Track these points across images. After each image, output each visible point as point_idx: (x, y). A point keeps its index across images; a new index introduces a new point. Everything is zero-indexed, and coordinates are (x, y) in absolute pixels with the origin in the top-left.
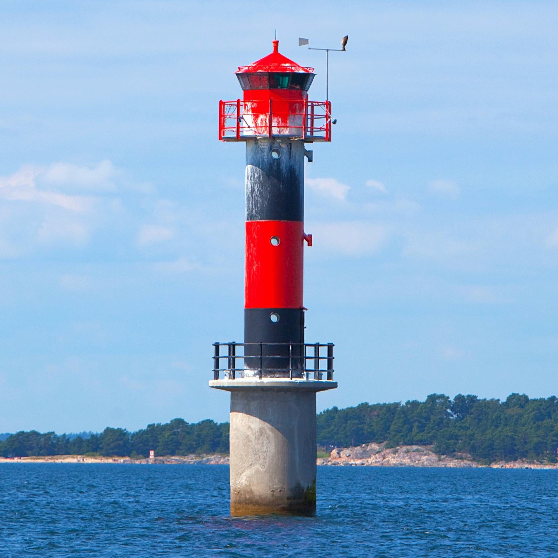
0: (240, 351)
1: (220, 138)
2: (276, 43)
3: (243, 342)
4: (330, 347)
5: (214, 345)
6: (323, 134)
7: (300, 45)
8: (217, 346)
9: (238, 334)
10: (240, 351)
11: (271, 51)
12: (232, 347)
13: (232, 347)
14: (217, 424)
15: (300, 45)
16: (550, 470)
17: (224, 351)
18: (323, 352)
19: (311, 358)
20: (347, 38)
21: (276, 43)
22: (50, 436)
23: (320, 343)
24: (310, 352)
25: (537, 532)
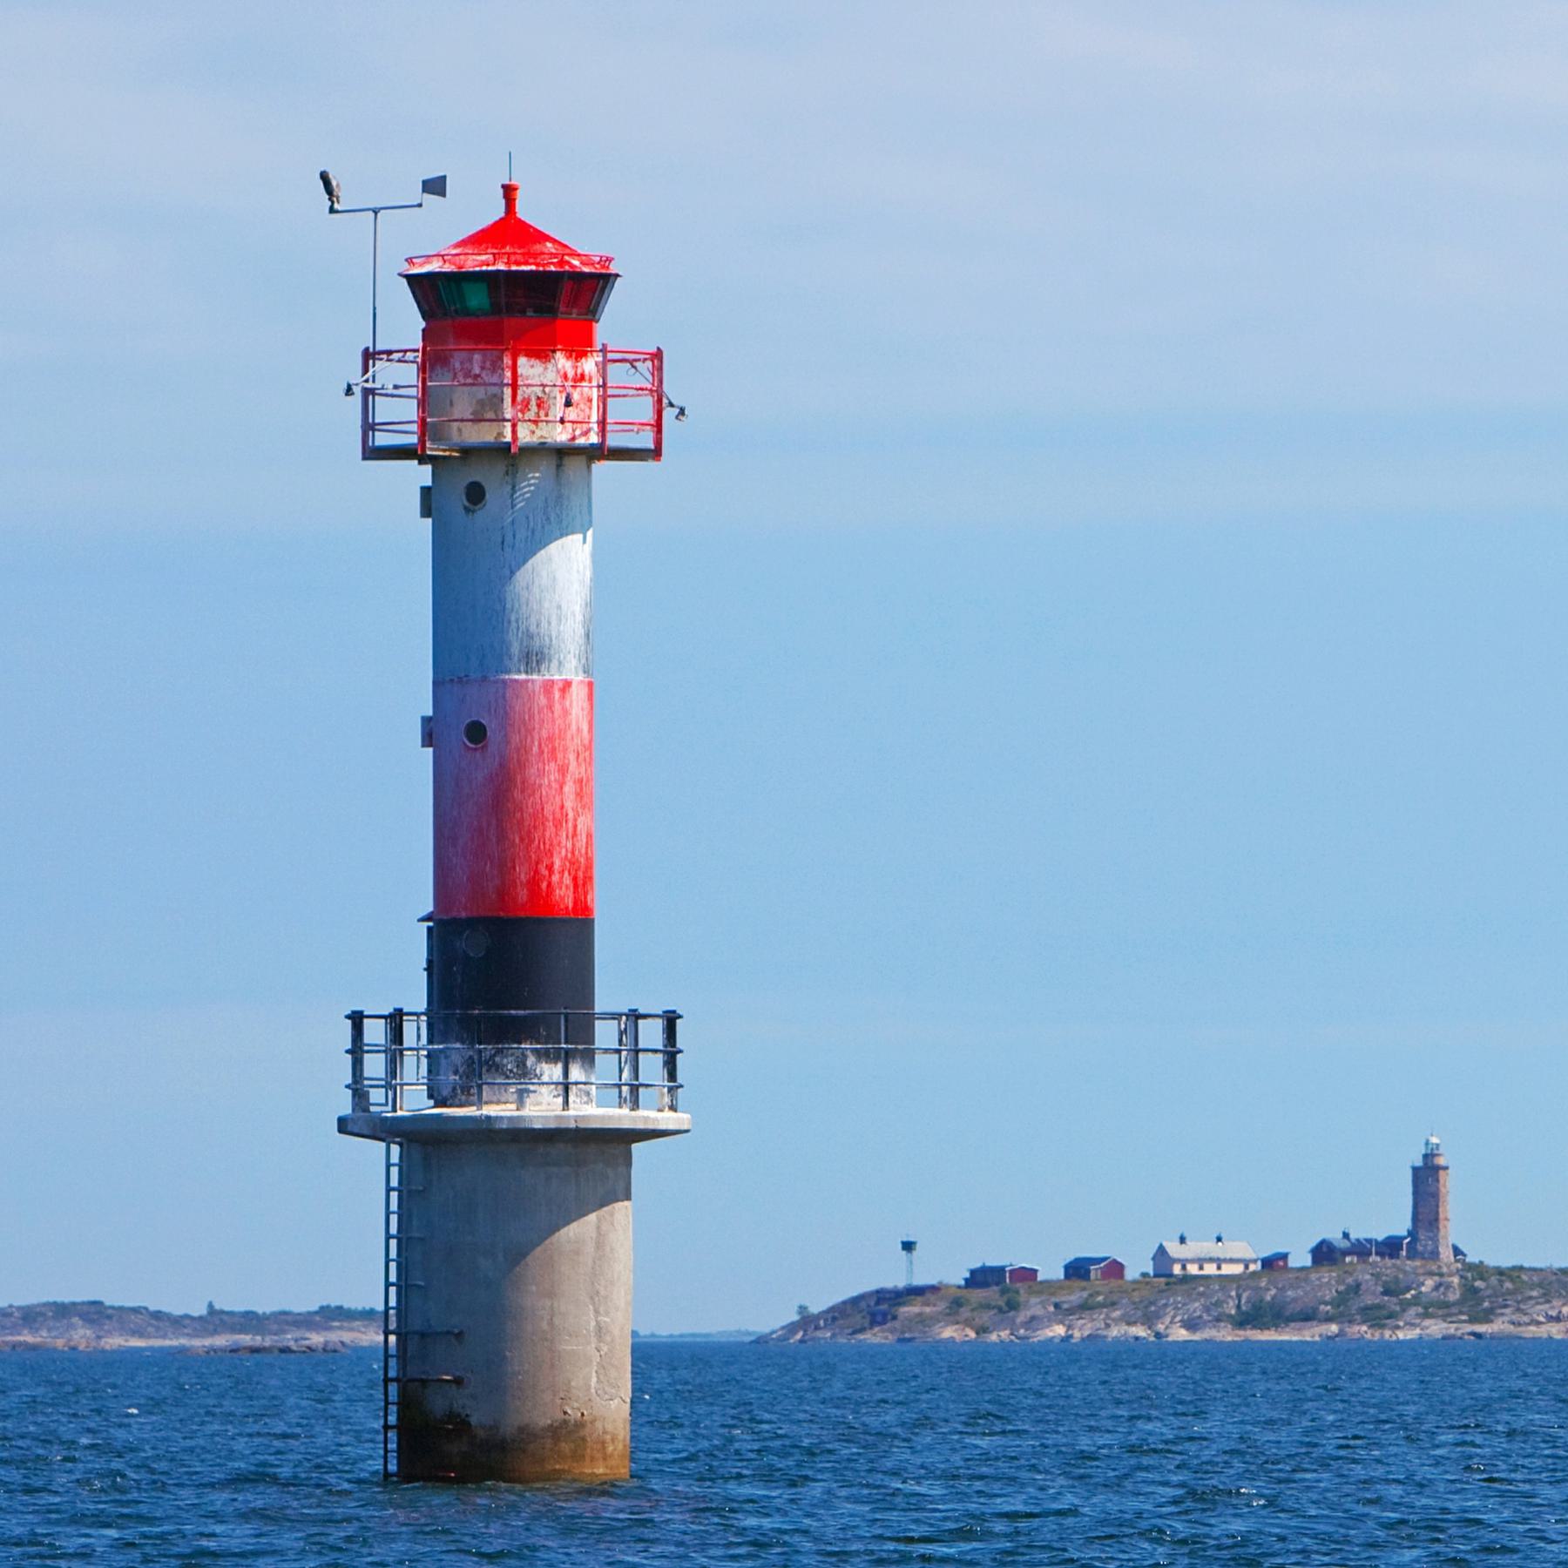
0: (413, 1033)
1: (656, 453)
2: (509, 192)
3: (422, 1005)
4: (671, 1021)
5: (348, 1017)
6: (646, 440)
7: (444, 195)
8: (357, 1019)
9: (412, 991)
10: (413, 1033)
11: (497, 211)
12: (395, 1020)
13: (395, 1020)
14: (1144, 1275)
15: (444, 195)
16: (1434, 1345)
17: (375, 1032)
18: (651, 1034)
19: (606, 1051)
20: (325, 178)
21: (509, 192)
22: (340, 1308)
23: (642, 1011)
24: (605, 1034)
25: (291, 1441)
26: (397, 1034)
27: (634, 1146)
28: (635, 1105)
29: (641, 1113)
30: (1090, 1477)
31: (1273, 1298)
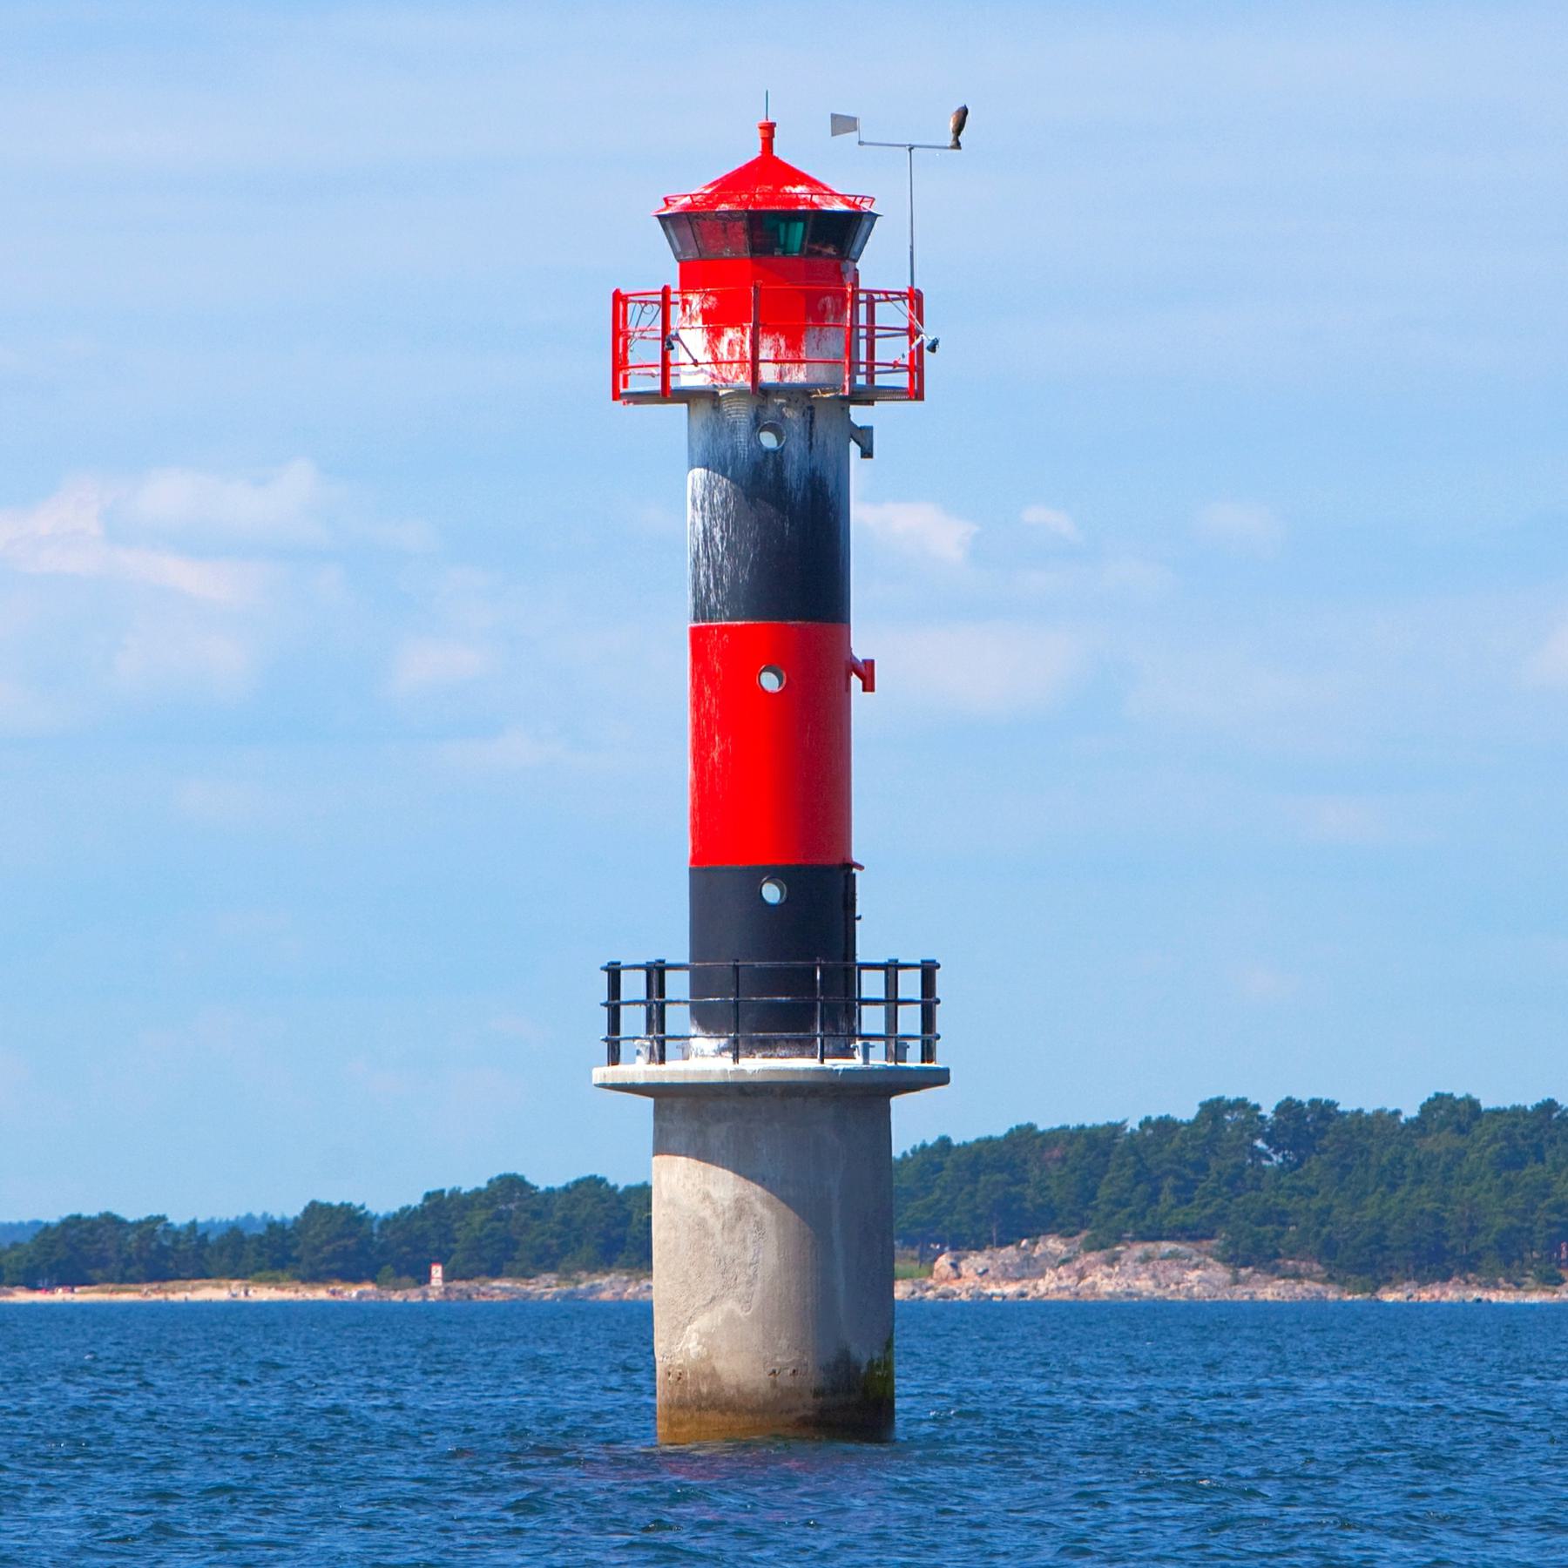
0: (678, 985)
1: (616, 395)
2: (769, 129)
3: (685, 958)
4: (928, 971)
8: (614, 972)
10: (678, 985)
11: (754, 151)
12: (656, 973)
13: (656, 973)
17: (634, 985)
18: (910, 985)
19: (876, 1002)
20: (964, 113)
21: (769, 129)
24: (872, 985)
26: (892, 984)
27: (893, 1100)
28: (662, 1060)
29: (670, 1065)
30: (1208, 1546)
31: (427, 1278)
